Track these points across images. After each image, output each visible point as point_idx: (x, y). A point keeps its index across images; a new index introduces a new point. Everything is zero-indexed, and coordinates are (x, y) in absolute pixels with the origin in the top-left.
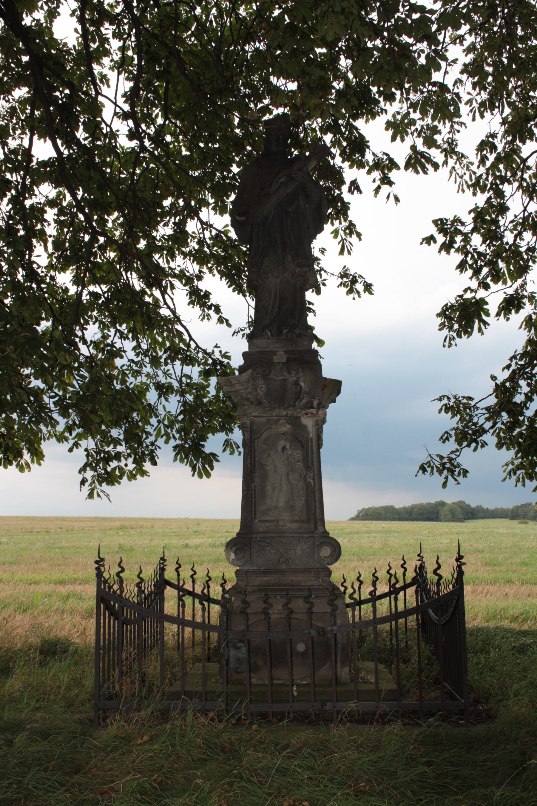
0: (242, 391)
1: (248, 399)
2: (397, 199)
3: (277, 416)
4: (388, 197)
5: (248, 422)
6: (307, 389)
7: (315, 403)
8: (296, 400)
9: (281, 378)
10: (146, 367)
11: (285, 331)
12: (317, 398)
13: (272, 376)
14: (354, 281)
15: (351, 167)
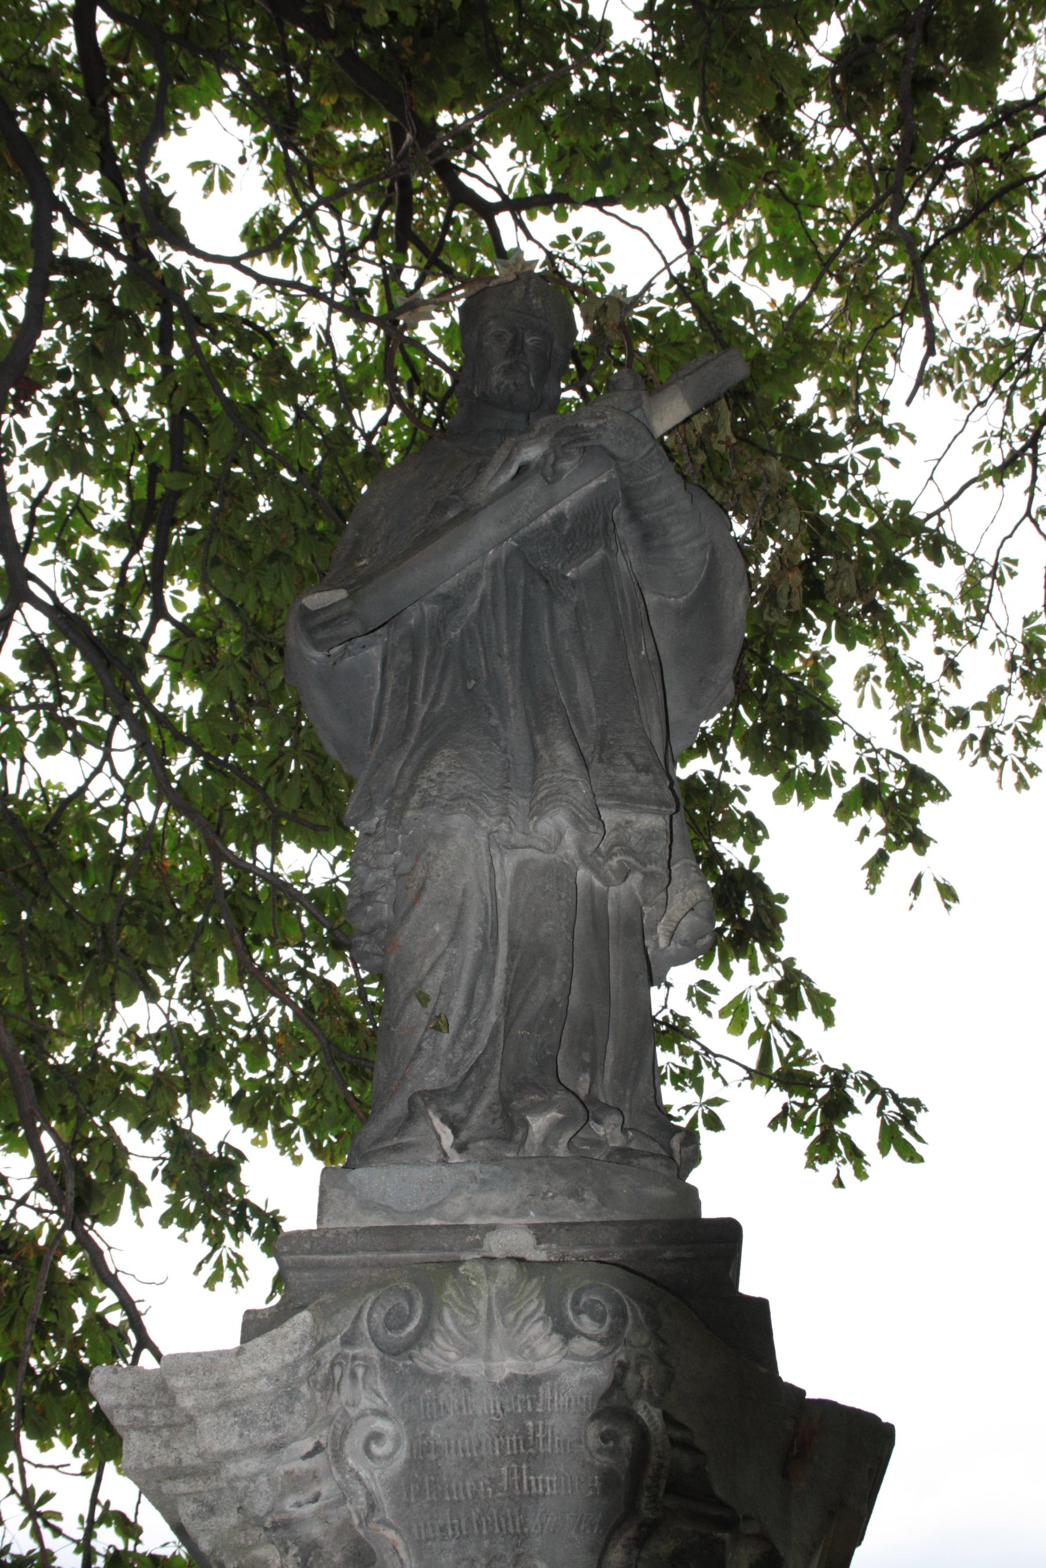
0: (250, 1465)
2: (947, 893)
4: (916, 888)
9: (507, 1366)
11: (538, 1124)
13: (442, 1355)
14: (838, 1106)
15: (780, 797)
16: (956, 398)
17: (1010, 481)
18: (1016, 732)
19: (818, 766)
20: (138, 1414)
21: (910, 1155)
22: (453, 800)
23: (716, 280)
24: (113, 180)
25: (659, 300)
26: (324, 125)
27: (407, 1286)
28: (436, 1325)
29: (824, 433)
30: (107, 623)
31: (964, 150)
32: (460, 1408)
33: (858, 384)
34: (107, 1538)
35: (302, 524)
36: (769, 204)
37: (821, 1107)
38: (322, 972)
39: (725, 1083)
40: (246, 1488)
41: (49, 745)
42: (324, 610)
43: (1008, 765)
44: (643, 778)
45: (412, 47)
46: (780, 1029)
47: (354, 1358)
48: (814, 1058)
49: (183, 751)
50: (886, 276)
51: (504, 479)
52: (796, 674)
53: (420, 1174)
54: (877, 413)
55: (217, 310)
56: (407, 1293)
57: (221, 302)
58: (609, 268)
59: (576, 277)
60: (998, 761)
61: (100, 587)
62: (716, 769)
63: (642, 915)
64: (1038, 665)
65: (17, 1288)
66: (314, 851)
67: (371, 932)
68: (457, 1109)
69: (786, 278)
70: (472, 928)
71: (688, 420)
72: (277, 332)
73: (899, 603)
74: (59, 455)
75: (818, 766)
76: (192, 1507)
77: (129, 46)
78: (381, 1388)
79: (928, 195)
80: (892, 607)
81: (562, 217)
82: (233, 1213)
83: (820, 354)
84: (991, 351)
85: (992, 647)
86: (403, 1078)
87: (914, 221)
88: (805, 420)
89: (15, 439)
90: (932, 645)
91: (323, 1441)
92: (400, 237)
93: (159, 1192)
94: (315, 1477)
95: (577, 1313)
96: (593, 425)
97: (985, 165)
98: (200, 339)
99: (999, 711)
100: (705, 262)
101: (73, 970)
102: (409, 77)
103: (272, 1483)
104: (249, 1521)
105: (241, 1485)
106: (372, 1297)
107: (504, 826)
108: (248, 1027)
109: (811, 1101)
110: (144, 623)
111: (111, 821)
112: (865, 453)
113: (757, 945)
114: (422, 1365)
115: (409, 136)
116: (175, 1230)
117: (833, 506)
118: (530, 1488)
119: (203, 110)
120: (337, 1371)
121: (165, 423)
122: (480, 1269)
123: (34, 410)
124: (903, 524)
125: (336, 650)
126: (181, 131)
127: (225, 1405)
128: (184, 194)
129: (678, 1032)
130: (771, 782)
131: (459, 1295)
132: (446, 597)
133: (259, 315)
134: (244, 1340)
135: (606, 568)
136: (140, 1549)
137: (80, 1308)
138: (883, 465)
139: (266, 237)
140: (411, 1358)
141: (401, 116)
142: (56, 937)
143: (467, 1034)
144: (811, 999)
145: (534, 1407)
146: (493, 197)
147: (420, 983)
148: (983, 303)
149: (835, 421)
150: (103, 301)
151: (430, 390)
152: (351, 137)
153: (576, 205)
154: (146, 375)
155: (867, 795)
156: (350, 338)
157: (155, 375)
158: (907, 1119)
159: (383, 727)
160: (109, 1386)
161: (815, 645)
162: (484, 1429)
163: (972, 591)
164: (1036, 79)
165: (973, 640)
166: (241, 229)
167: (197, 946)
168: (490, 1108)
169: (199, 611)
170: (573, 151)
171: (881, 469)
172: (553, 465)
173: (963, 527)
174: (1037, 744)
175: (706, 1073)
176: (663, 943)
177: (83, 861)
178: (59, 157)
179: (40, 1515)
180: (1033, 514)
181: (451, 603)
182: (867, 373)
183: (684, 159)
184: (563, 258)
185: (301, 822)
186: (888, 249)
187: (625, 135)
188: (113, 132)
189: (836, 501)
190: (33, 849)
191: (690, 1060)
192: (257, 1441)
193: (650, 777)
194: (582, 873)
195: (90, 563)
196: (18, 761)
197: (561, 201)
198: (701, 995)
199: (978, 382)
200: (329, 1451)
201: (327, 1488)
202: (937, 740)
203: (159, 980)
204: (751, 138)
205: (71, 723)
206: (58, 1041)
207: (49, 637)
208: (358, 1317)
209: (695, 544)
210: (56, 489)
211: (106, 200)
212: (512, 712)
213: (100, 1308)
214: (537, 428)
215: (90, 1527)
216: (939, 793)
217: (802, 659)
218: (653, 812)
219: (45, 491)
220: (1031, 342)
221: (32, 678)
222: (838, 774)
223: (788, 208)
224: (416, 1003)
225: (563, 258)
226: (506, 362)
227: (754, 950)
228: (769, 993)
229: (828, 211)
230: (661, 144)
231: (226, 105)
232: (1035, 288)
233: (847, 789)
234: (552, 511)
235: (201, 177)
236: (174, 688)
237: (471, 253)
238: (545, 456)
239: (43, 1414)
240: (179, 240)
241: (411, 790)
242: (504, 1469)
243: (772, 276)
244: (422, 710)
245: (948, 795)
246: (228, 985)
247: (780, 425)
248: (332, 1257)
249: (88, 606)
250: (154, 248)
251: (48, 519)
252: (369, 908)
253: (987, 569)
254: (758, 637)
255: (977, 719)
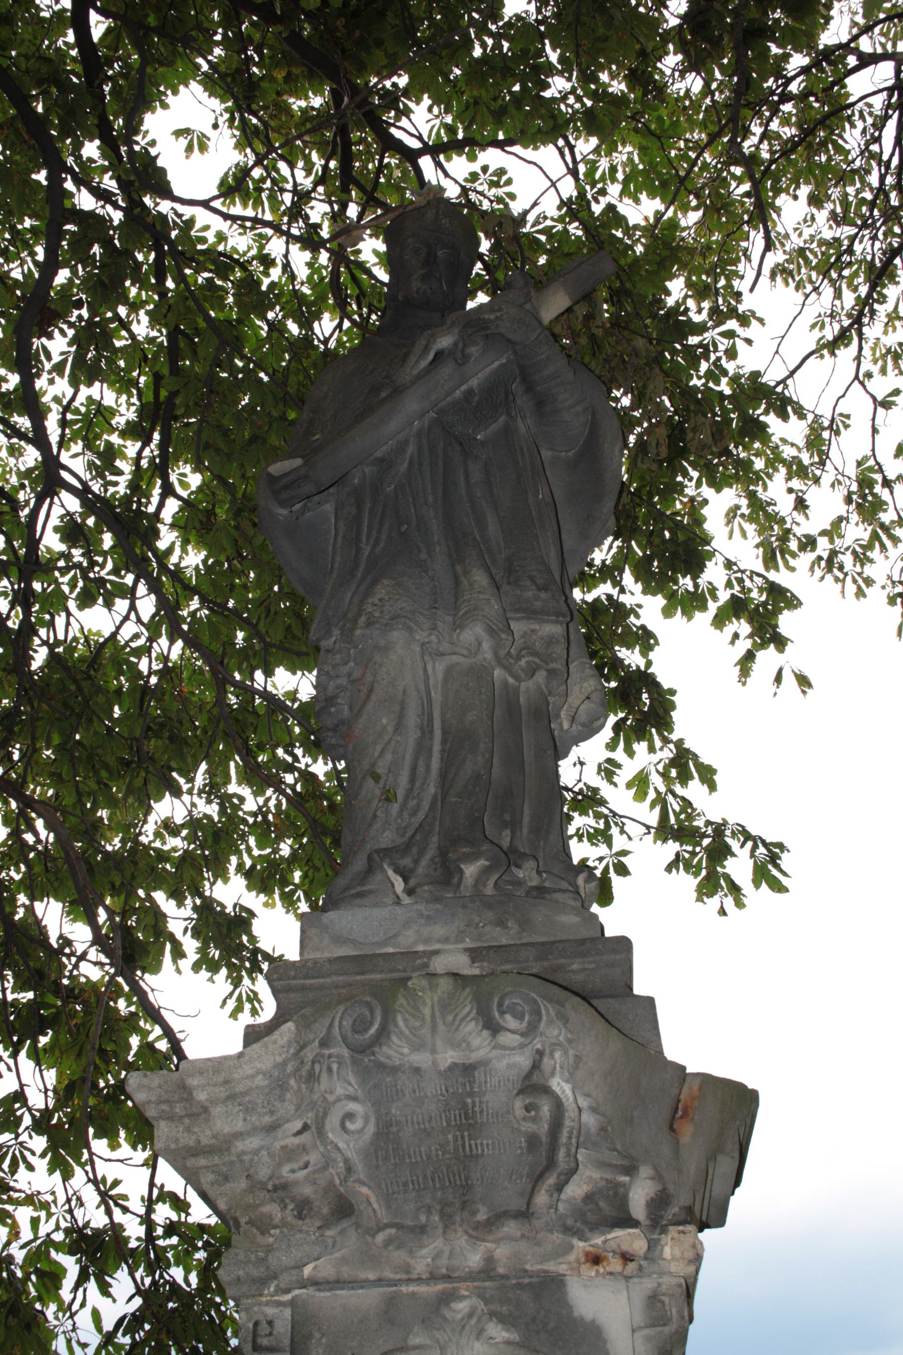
0: (253, 1143)
1: (280, 1190)
2: (803, 681)
3: (434, 1277)
4: (778, 679)
5: (283, 1319)
6: (590, 1120)
7: (639, 1195)
8: (538, 1179)
9: (449, 1057)
10: (30, 1168)
11: (470, 870)
12: (645, 1171)
13: (398, 1050)
14: (719, 852)
15: (668, 612)
16: (797, 288)
17: (842, 352)
18: (854, 553)
19: (696, 586)
20: (165, 1107)
21: (778, 887)
22: (392, 619)
23: (597, 202)
24: (110, 146)
25: (552, 219)
26: (279, 94)
27: (368, 998)
28: (392, 1027)
29: (690, 320)
30: (126, 500)
31: (794, 88)
32: (414, 1091)
33: (716, 281)
34: (163, 1213)
35: (275, 413)
36: (638, 139)
37: (705, 852)
38: (307, 766)
39: (630, 838)
40: (251, 1160)
41: (86, 600)
42: (285, 475)
43: (849, 579)
44: (543, 595)
45: (345, 27)
46: (675, 795)
47: (330, 1056)
48: (699, 815)
49: (192, 599)
50: (736, 192)
51: (424, 364)
52: (677, 513)
53: (378, 913)
54: (733, 303)
55: (199, 247)
56: (369, 1005)
57: (204, 240)
58: (512, 196)
59: (486, 205)
60: (841, 576)
61: (120, 473)
62: (615, 592)
63: (548, 704)
64: (870, 498)
65: (84, 1024)
66: (299, 673)
67: (335, 729)
68: (407, 862)
69: (653, 198)
70: (412, 719)
71: (569, 310)
72: (249, 262)
73: (757, 455)
74: (83, 371)
75: (696, 586)
76: (211, 1177)
77: (118, 38)
78: (352, 1078)
79: (767, 125)
80: (753, 458)
81: (472, 158)
82: (248, 959)
83: (685, 258)
84: (823, 249)
85: (833, 485)
86: (363, 840)
87: (757, 147)
88: (675, 311)
89: (43, 358)
90: (784, 487)
91: (309, 1122)
92: (342, 183)
93: (190, 945)
94: (304, 1149)
95: (502, 1013)
96: (492, 317)
97: (812, 99)
98: (188, 271)
99: (841, 536)
100: (588, 187)
101: (115, 775)
102: (343, 51)
103: (271, 1155)
104: (256, 1185)
105: (246, 1158)
106: (341, 1008)
107: (433, 638)
108: (254, 814)
109: (698, 849)
110: (155, 500)
111: (140, 659)
112: (722, 334)
113: (653, 730)
114: (382, 1059)
115: (346, 99)
116: (204, 974)
117: (699, 378)
118: (471, 1150)
119: (182, 88)
120: (317, 1067)
121: (163, 340)
122: (424, 983)
123: (57, 333)
124: (754, 390)
125: (297, 507)
126: (165, 106)
127: (231, 1097)
128: (170, 156)
129: (589, 800)
130: (660, 601)
131: (409, 1004)
132: (381, 460)
133: (234, 250)
134: (245, 1047)
135: (508, 431)
136: (190, 1220)
137: (135, 1041)
138: (740, 345)
139: (235, 186)
140: (373, 1054)
141: (338, 82)
142: (100, 751)
143: (412, 803)
144: (697, 771)
145: (472, 1087)
146: (415, 144)
147: (373, 765)
148: (815, 211)
149: (699, 311)
150: (107, 243)
151: (375, 303)
152: (303, 104)
153: (483, 147)
154: (147, 302)
155: (737, 607)
156: (307, 264)
157: (154, 302)
158: (774, 859)
159: (336, 565)
160: (140, 1086)
161: (690, 491)
162: (433, 1107)
163: (815, 442)
164: (851, 27)
165: (817, 480)
166: (218, 182)
167: (211, 752)
168: (432, 860)
169: (200, 489)
170: (476, 103)
171: (738, 348)
172: (463, 351)
173: (802, 390)
174: (871, 561)
175: (615, 831)
176: (566, 726)
177: (119, 690)
178: (66, 131)
179: (111, 1197)
180: (861, 378)
181: (385, 464)
182: (723, 270)
183: (567, 106)
184: (475, 191)
185: (286, 650)
186: (738, 171)
187: (517, 88)
188: (109, 110)
189: (702, 374)
190: (75, 681)
191: (602, 821)
192: (258, 1124)
193: (549, 594)
194: (498, 673)
195: (110, 455)
196: (63, 614)
197: (470, 145)
198: (609, 770)
199: (814, 275)
200: (313, 1129)
201: (313, 1158)
202: (792, 562)
203: (182, 781)
204: (623, 87)
205: (101, 582)
206: (108, 834)
207: (81, 514)
208: (331, 1025)
209: (579, 408)
210: (81, 398)
211: (106, 163)
212: (438, 549)
213: (151, 1038)
214: (449, 322)
215: (149, 1204)
216: (793, 602)
217: (681, 502)
218: (552, 622)
219: (73, 399)
220: (852, 239)
221: (69, 548)
222: (713, 591)
223: (655, 139)
224: (370, 781)
225: (475, 191)
226: (423, 271)
227: (651, 734)
228: (664, 768)
229: (687, 141)
230: (547, 94)
231: (199, 82)
232: (856, 196)
233: (721, 603)
234: (464, 388)
235: (183, 142)
236: (184, 551)
237: (401, 191)
238: (455, 344)
239: (107, 1119)
240: (165, 192)
241: (359, 615)
242: (450, 1136)
243: (643, 197)
244: (366, 551)
245: (800, 604)
246: (239, 783)
247: (654, 316)
248: (312, 981)
249: (111, 490)
250: (147, 200)
251: (76, 422)
252: (333, 709)
253: (826, 424)
254: (644, 486)
255: (823, 545)
